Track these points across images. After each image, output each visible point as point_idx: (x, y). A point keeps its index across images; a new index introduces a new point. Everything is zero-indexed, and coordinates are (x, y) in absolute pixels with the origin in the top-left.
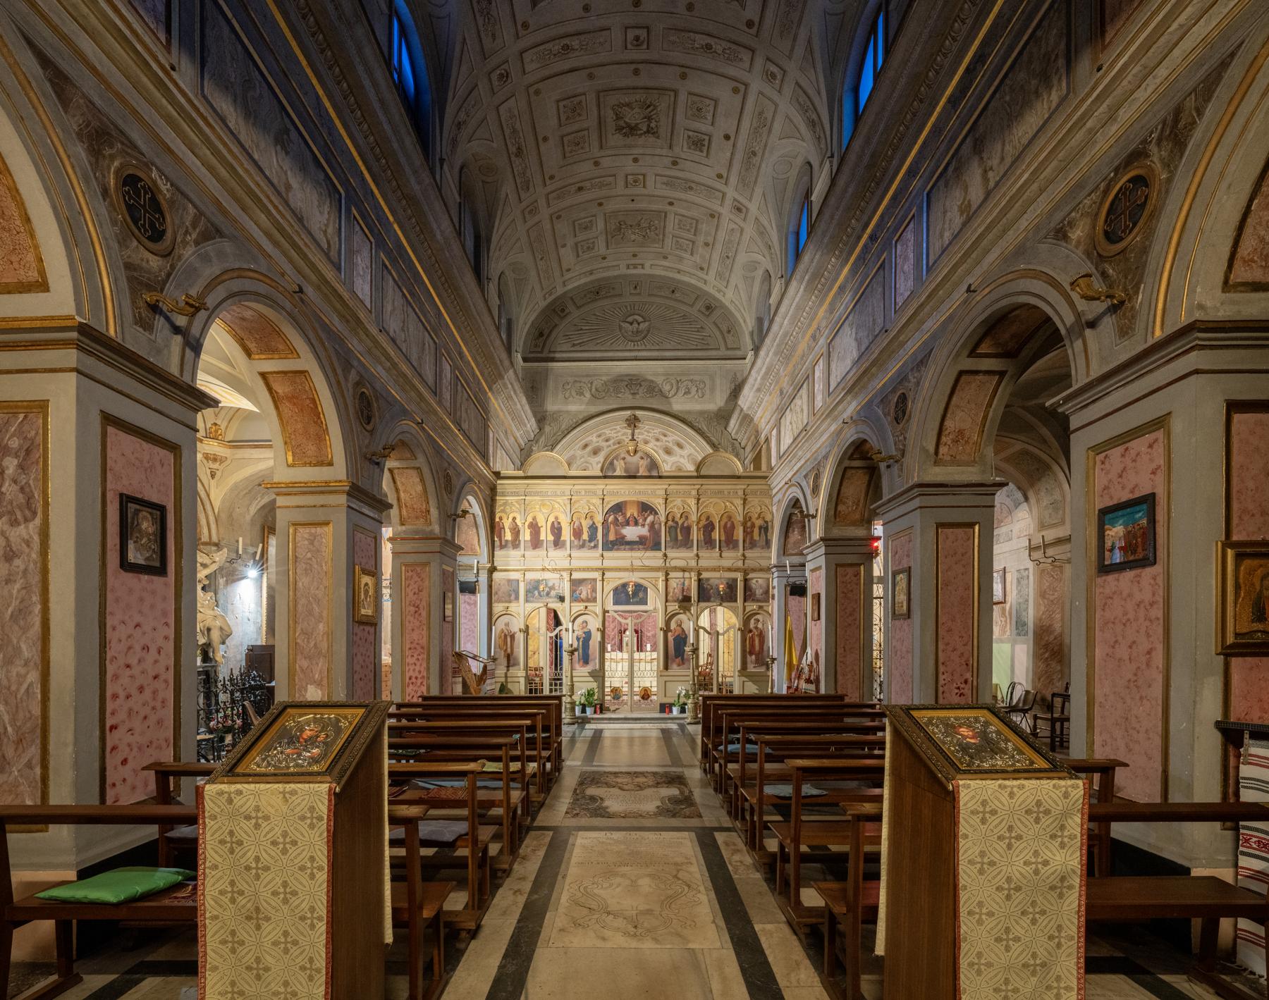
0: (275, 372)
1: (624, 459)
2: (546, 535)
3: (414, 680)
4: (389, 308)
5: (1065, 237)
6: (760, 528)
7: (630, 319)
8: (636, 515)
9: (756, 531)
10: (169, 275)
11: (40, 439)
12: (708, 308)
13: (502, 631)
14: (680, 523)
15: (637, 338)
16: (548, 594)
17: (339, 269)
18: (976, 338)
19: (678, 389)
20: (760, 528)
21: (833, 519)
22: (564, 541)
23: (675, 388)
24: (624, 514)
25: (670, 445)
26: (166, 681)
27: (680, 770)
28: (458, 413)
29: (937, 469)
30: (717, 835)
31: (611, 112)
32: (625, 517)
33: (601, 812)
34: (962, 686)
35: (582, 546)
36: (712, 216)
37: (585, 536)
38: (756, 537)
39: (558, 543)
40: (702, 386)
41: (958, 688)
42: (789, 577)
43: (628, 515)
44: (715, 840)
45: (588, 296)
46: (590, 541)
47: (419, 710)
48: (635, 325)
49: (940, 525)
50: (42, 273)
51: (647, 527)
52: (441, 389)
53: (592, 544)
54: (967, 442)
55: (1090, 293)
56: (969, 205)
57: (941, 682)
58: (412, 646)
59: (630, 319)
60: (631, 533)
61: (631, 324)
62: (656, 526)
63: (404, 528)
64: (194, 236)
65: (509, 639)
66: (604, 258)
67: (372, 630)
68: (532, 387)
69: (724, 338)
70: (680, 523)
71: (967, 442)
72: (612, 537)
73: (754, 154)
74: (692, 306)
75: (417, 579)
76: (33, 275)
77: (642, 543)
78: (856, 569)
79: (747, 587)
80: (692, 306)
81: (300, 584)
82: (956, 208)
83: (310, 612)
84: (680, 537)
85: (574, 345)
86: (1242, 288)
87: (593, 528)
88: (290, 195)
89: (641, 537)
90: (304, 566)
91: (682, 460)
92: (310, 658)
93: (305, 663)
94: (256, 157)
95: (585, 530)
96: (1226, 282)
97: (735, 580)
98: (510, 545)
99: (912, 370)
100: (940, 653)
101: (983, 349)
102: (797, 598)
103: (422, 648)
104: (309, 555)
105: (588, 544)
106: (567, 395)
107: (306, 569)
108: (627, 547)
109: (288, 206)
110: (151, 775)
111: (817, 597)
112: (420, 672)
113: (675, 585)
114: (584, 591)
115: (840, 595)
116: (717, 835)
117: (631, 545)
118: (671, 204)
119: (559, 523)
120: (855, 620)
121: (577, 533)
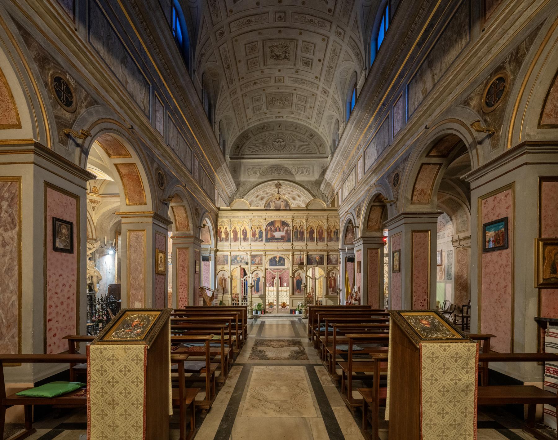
0: (121, 164)
1: (274, 202)
2: (240, 236)
3: (182, 299)
4: (171, 135)
5: (468, 104)
6: (334, 232)
7: (277, 140)
8: (279, 227)
9: (333, 234)
10: (74, 121)
11: (17, 193)
12: (311, 135)
13: (221, 278)
14: (299, 230)
15: (280, 149)
16: (241, 261)
17: (149, 118)
18: (429, 149)
19: (298, 171)
20: (334, 232)
21: (366, 228)
22: (248, 238)
23: (297, 171)
24: (274, 226)
25: (295, 196)
26: (73, 300)
27: (299, 339)
28: (202, 182)
29: (412, 207)
30: (315, 367)
31: (269, 49)
32: (275, 227)
33: (264, 357)
34: (423, 302)
35: (256, 240)
36: (313, 95)
37: (257, 236)
38: (332, 236)
39: (245, 239)
40: (309, 170)
41: (421, 303)
42: (347, 254)
43: (276, 227)
44: (314, 370)
45: (259, 130)
46: (260, 238)
47: (184, 312)
48: (279, 143)
49: (413, 231)
50: (19, 120)
51: (284, 232)
52: (194, 171)
53: (260, 240)
54: (425, 194)
55: (479, 129)
56: (426, 90)
57: (414, 300)
58: (181, 284)
59: (277, 140)
60: (277, 234)
61: (278, 142)
62: (289, 232)
63: (177, 232)
64: (85, 104)
65: (224, 281)
66: (266, 114)
67: (164, 277)
68: (234, 170)
69: (318, 149)
70: (299, 230)
71: (425, 194)
72: (269, 236)
73: (332, 68)
74: (304, 135)
75: (183, 255)
76: (15, 121)
77: (282, 239)
78: (376, 250)
79: (328, 258)
80: (304, 135)
81: (132, 257)
82: (420, 92)
83: (136, 269)
84: (299, 236)
85: (252, 152)
86: (546, 127)
87: (261, 232)
88: (128, 86)
89: (282, 236)
90: (134, 249)
91: (300, 202)
92: (136, 289)
93: (134, 292)
94: (113, 69)
95: (257, 233)
96: (539, 124)
97: (323, 255)
98: (224, 240)
99: (401, 163)
100: (413, 288)
101: (432, 154)
102: (351, 263)
103: (186, 285)
104: (136, 244)
105: (258, 239)
106: (249, 174)
107: (134, 251)
108: (276, 241)
109: (127, 90)
110: (67, 341)
111: (359, 263)
112: (185, 296)
113: (297, 258)
114: (257, 260)
115: (369, 262)
116: (315, 367)
117: (277, 240)
118: (295, 90)
119: (246, 230)
120: (376, 273)
121: (254, 235)
